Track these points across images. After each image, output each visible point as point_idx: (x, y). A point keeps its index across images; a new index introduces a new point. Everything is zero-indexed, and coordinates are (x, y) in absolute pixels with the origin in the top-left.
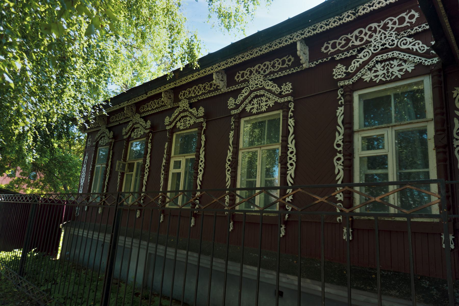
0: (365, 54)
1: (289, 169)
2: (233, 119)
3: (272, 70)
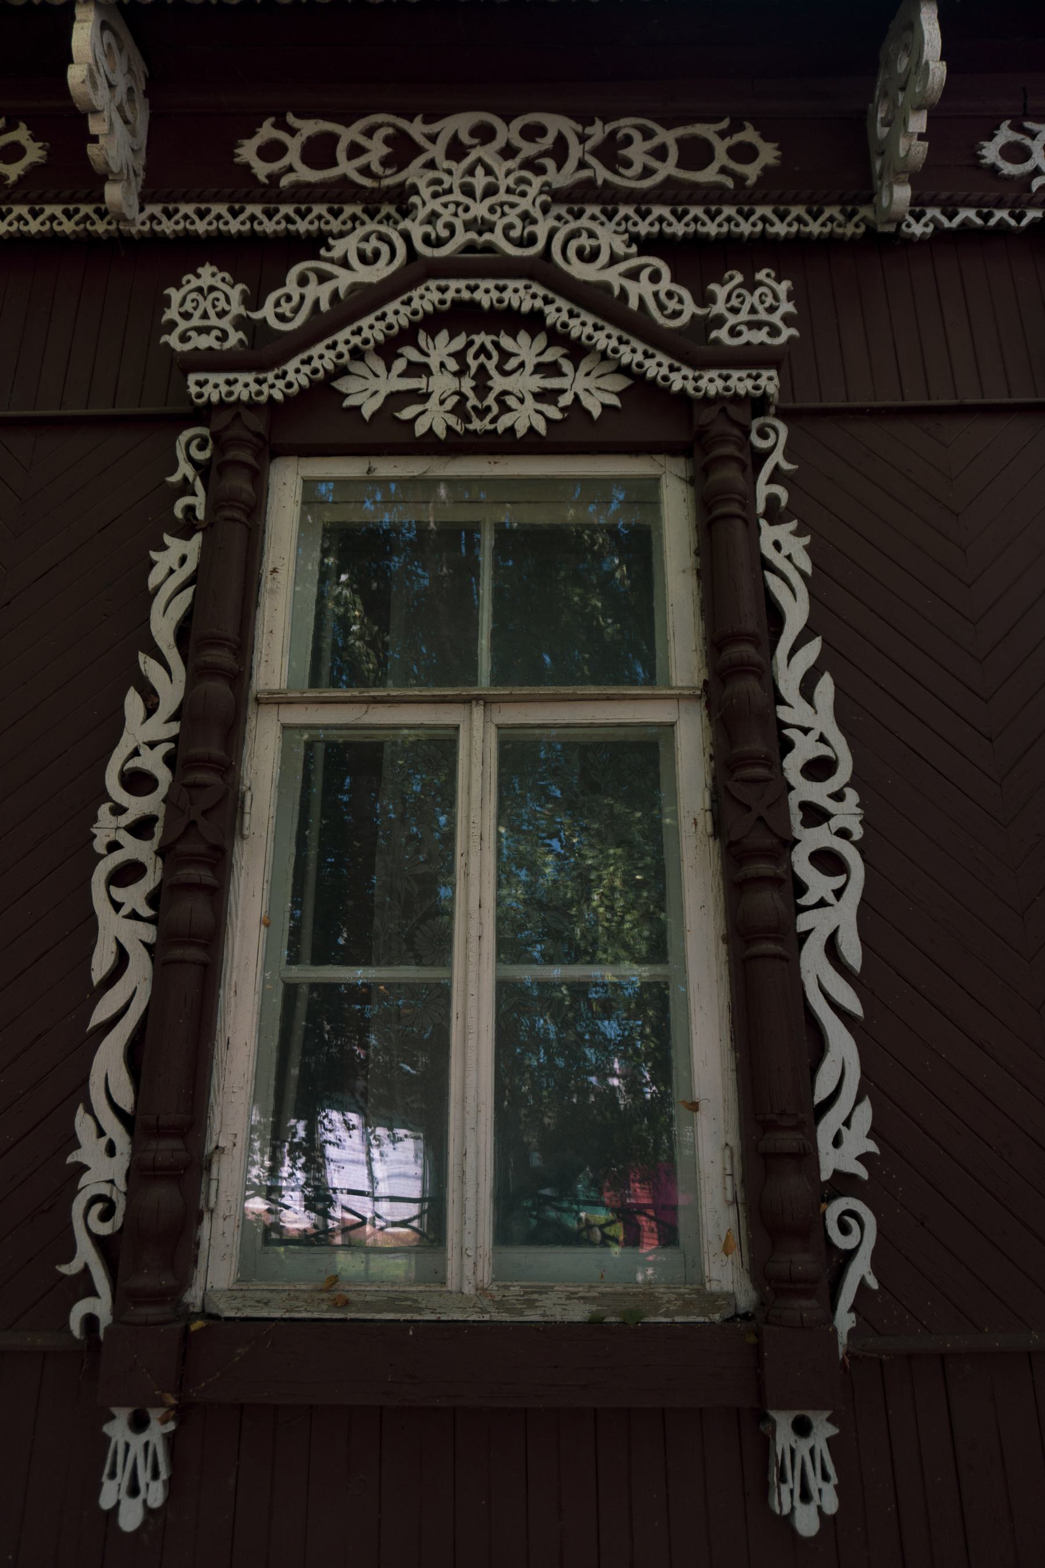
0: (368, 248)
1: (806, 900)
2: (188, 449)
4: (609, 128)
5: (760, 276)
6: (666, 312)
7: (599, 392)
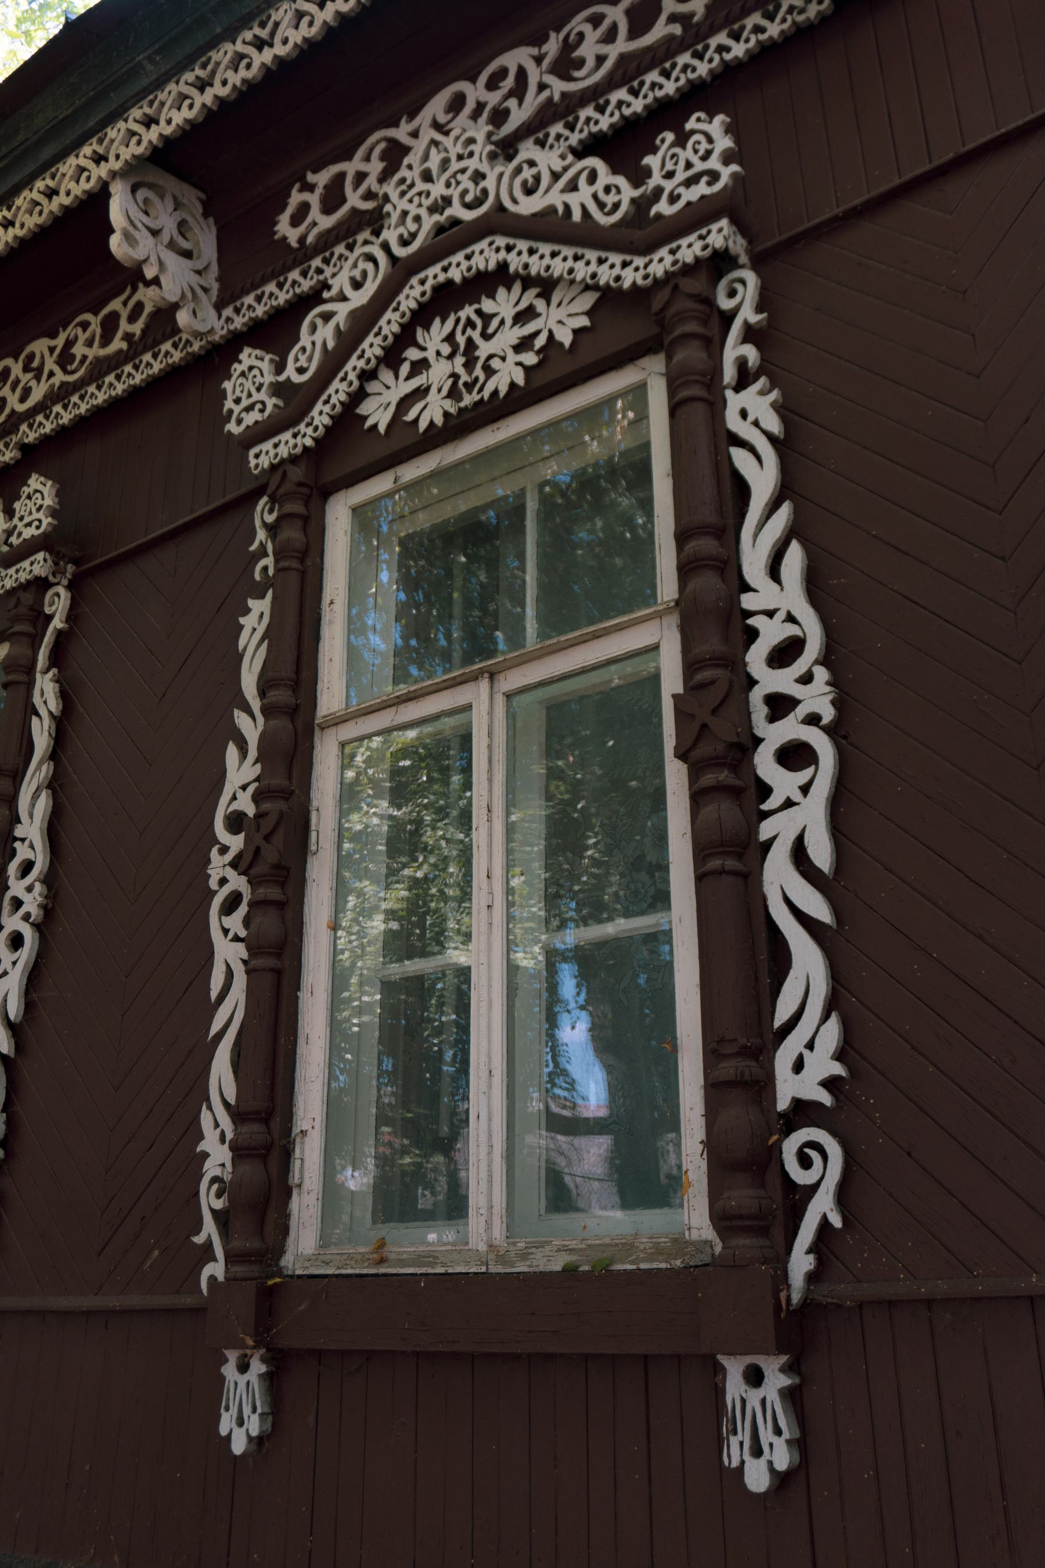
3: (558, 87)
4: (562, 35)
5: (691, 124)
6: (606, 210)
7: (570, 319)
